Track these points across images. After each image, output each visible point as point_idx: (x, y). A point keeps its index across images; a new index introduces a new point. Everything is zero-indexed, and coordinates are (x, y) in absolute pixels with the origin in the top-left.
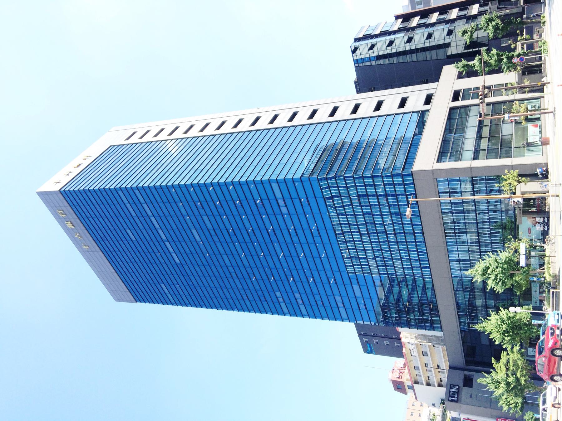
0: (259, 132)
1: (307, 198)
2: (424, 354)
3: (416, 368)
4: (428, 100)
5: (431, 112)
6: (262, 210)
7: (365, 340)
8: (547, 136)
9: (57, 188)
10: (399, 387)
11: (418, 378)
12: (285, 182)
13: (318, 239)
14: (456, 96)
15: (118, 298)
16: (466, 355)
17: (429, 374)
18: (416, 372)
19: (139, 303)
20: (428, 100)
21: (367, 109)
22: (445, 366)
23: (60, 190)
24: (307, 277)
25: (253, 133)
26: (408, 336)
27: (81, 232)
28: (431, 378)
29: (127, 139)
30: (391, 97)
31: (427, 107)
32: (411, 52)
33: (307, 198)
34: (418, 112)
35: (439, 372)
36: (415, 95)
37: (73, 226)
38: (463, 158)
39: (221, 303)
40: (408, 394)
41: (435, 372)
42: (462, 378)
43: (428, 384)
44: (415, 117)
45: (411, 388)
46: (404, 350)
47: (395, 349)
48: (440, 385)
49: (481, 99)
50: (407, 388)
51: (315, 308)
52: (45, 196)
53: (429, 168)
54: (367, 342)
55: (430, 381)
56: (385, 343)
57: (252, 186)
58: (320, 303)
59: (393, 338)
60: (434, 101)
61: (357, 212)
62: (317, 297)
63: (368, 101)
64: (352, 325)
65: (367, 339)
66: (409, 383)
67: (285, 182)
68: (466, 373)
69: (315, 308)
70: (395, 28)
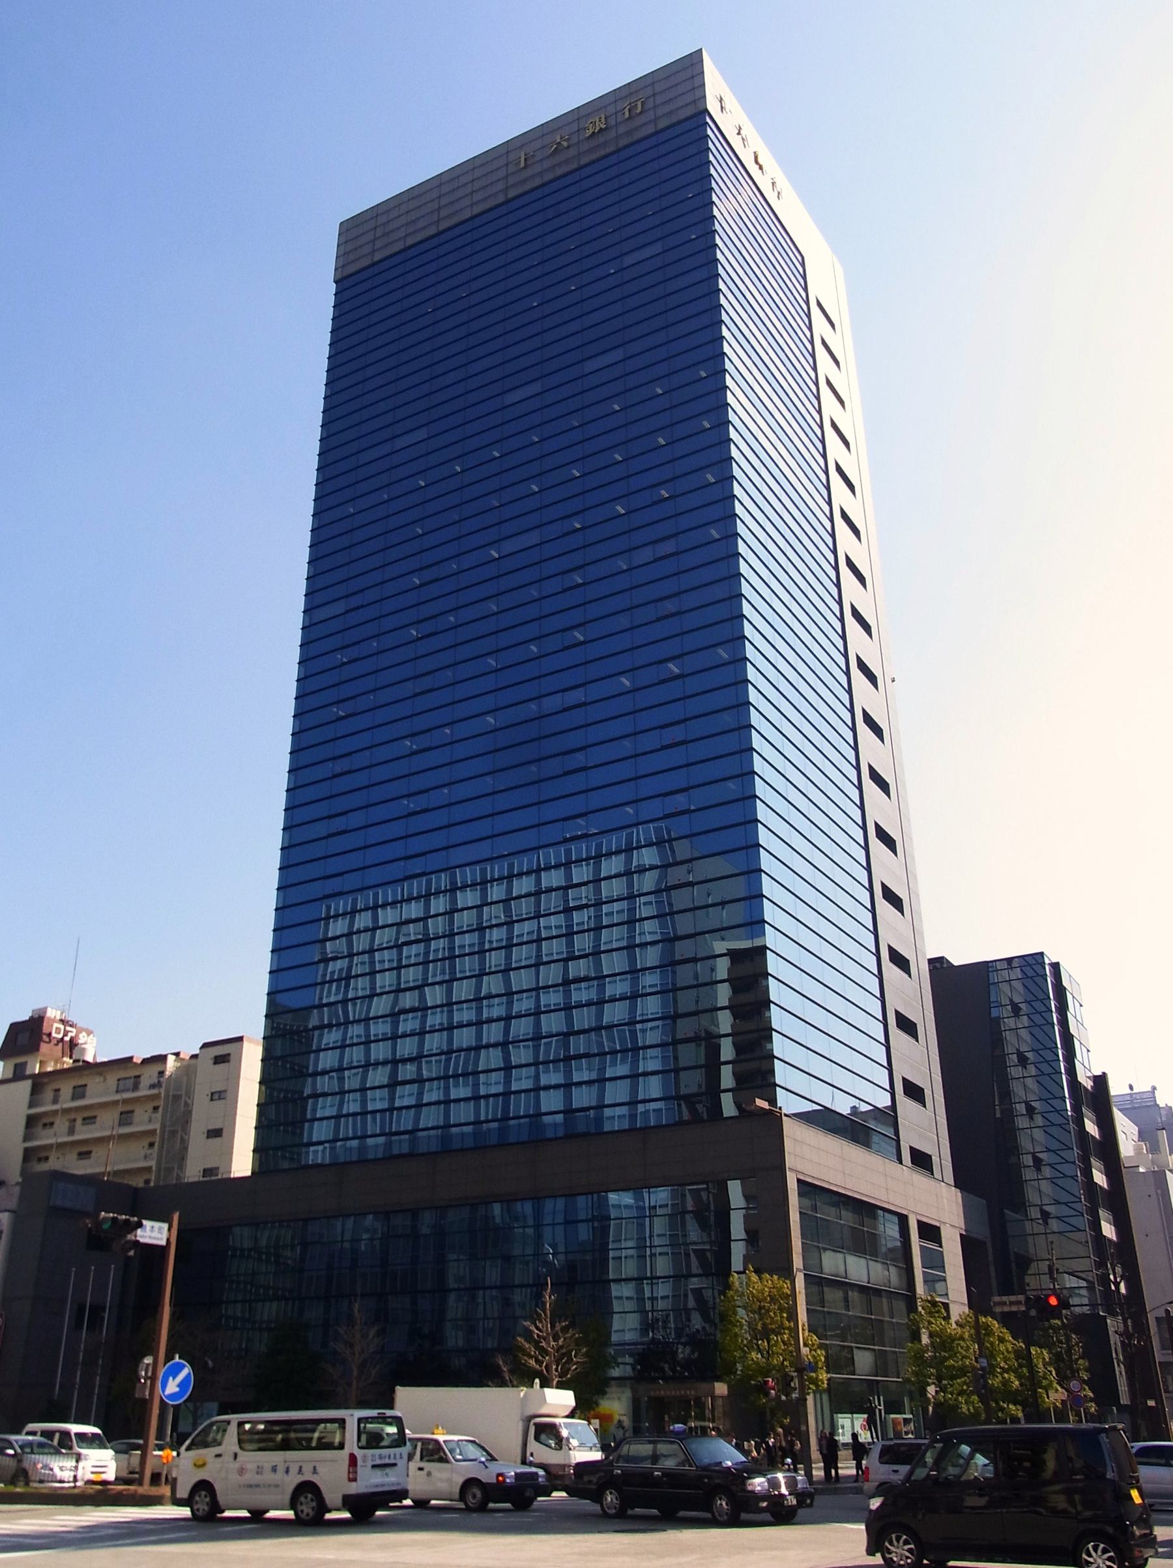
4: (921, 1161)
6: (649, 676)
9: (712, 106)
19: (333, 287)
20: (921, 1161)
23: (707, 111)
24: (434, 617)
27: (573, 152)
36: (927, 1126)
39: (337, 513)
45: (19, 1074)
51: (321, 809)
52: (693, 63)
53: (789, 1161)
56: (1138, 1533)
57: (723, 654)
58: (339, 824)
60: (919, 1179)
61: (399, 1118)
62: (357, 819)
69: (321, 809)
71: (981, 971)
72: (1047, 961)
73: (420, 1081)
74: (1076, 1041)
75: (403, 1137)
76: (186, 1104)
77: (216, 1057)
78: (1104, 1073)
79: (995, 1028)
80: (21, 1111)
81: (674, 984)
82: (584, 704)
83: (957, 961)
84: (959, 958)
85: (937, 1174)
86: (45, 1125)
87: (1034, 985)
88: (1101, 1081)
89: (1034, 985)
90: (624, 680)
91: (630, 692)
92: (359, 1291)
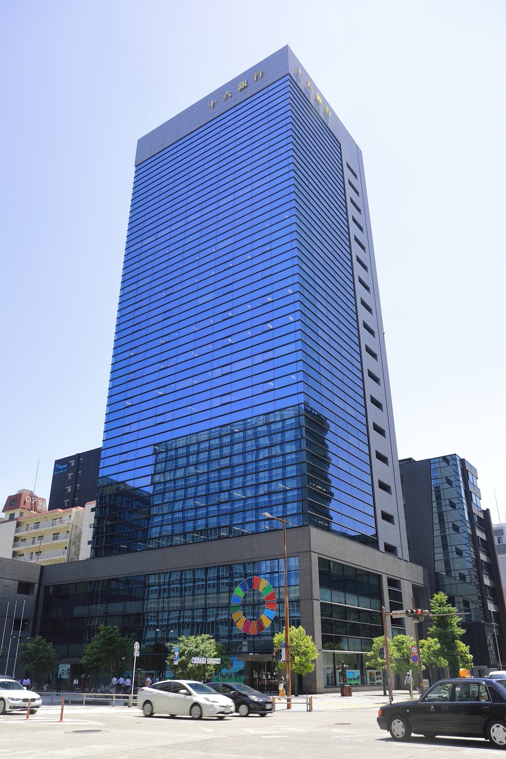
0: (356, 332)
1: (274, 390)
2: (56, 536)
3: (37, 525)
4: (390, 549)
5: (378, 552)
7: (73, 463)
8: (353, 693)
10: (13, 502)
11: (24, 527)
12: (107, 431)
13: (259, 389)
14: (393, 583)
15: (142, 143)
16: (58, 587)
17: (29, 540)
18: (32, 525)
19: (134, 169)
20: (390, 549)
21: (382, 472)
22: (43, 561)
25: (355, 324)
26: (84, 517)
28: (23, 543)
29: (348, 166)
30: (393, 503)
31: (382, 547)
32: (443, 529)
33: (274, 390)
34: (376, 535)
35: (32, 553)
36: (395, 533)
37: (242, 89)
38: (322, 589)
40: (4, 514)
41: (33, 548)
42: (32, 581)
43: (16, 539)
44: (370, 532)
45: (12, 518)
46: (60, 510)
47: (62, 496)
48: (15, 554)
49: (412, 612)
50: (12, 512)
54: (69, 464)
55: (19, 542)
59: (74, 498)
60: (389, 557)
63: (388, 474)
64: (99, 444)
65: (73, 464)
66: (17, 516)
67: (107, 431)
68: (37, 585)
70: (475, 510)
71: (427, 464)
72: (457, 458)
73: (284, 479)
74: (473, 496)
75: (290, 476)
76: (80, 529)
77: (92, 509)
78: (488, 509)
79: (437, 488)
80: (12, 535)
81: (184, 531)
82: (273, 359)
83: (417, 458)
84: (419, 456)
85: (400, 555)
86: (22, 540)
87: (456, 471)
88: (487, 513)
89: (456, 471)
90: (290, 318)
91: (293, 322)
92: (178, 586)
